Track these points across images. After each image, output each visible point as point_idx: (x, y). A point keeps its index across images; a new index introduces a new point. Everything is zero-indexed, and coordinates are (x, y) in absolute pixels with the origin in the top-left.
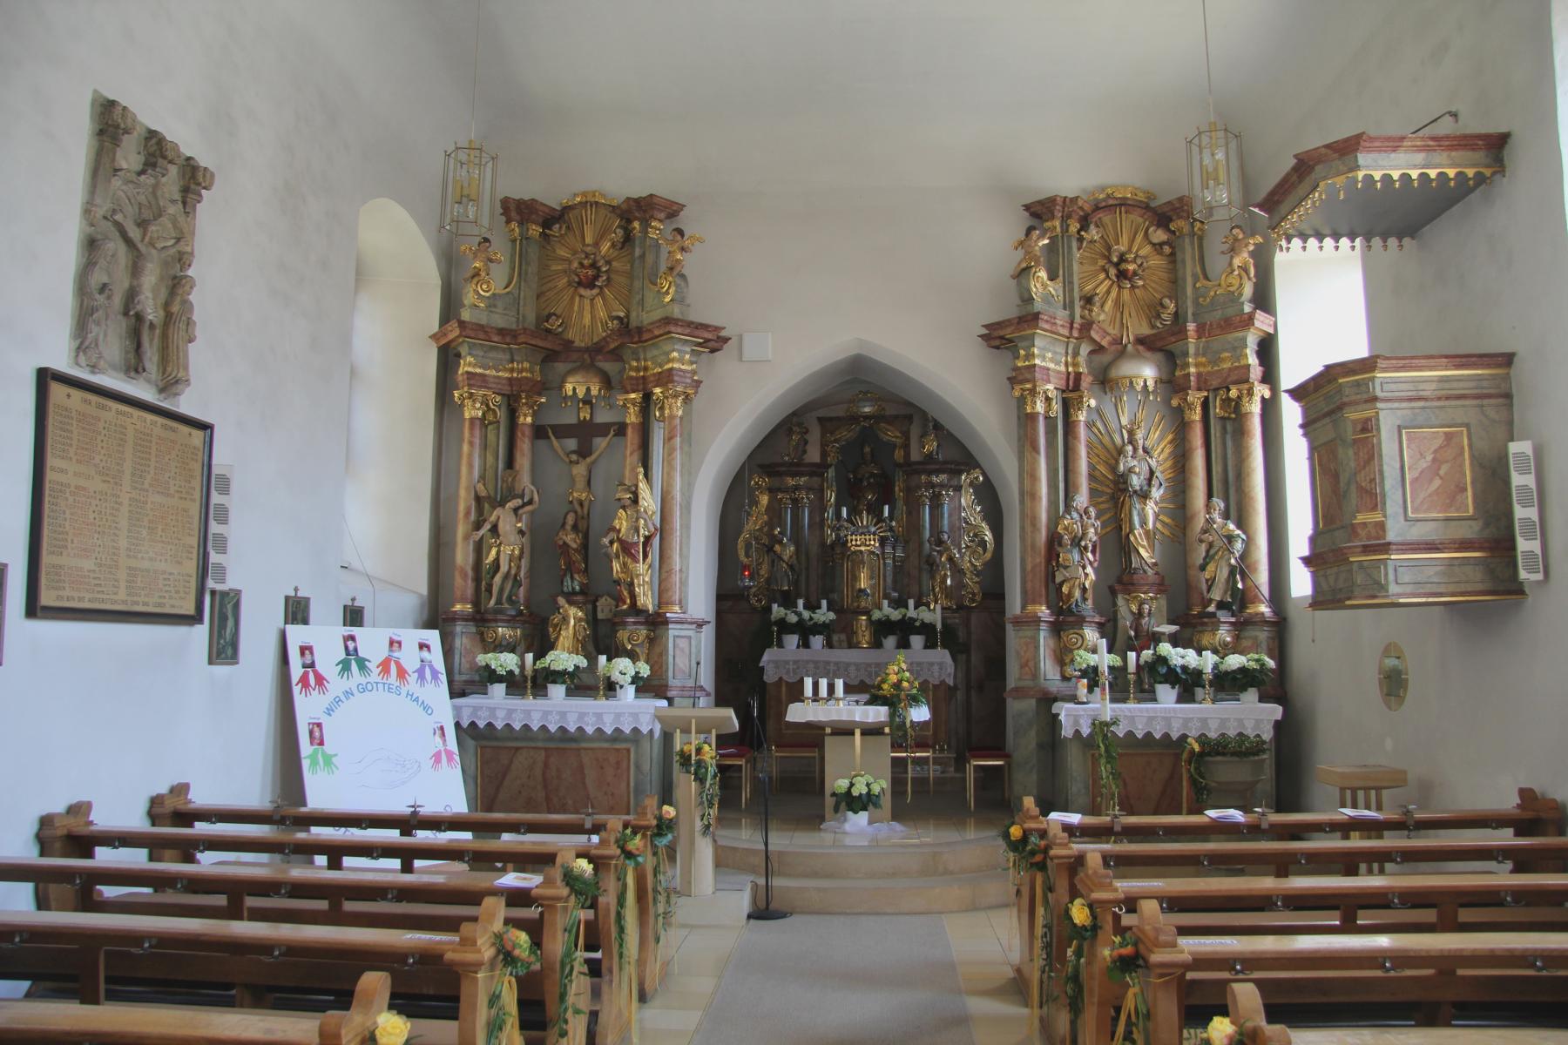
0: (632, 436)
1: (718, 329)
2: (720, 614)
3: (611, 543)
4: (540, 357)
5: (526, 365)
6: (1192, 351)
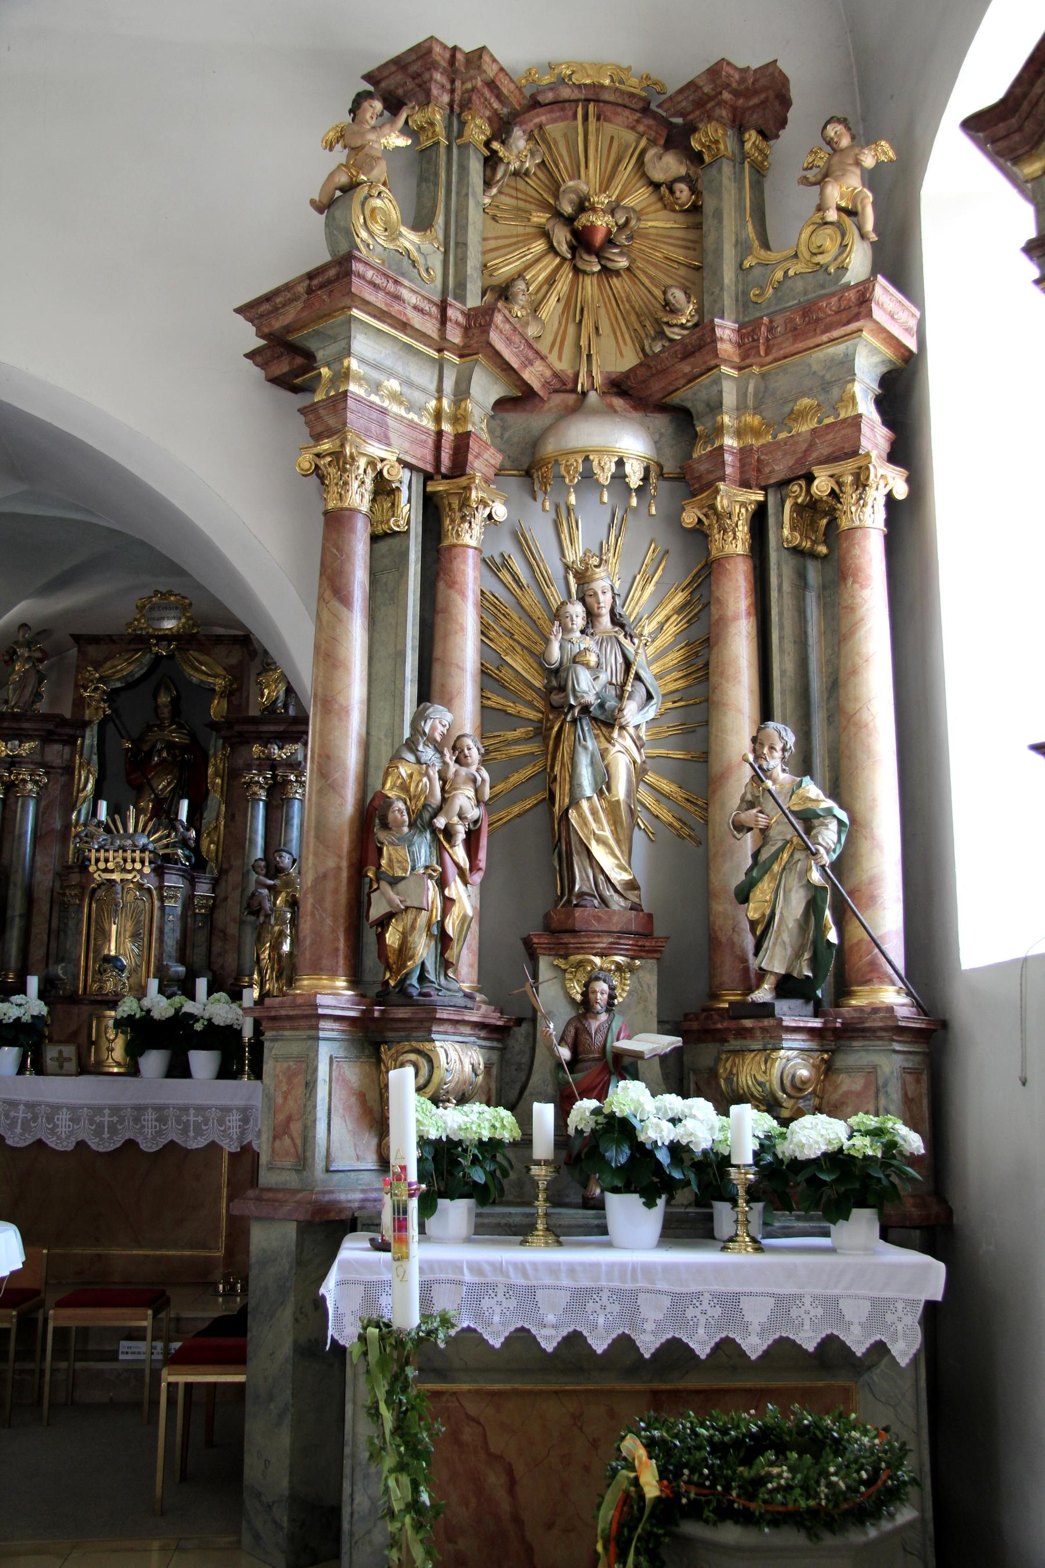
6: (730, 397)
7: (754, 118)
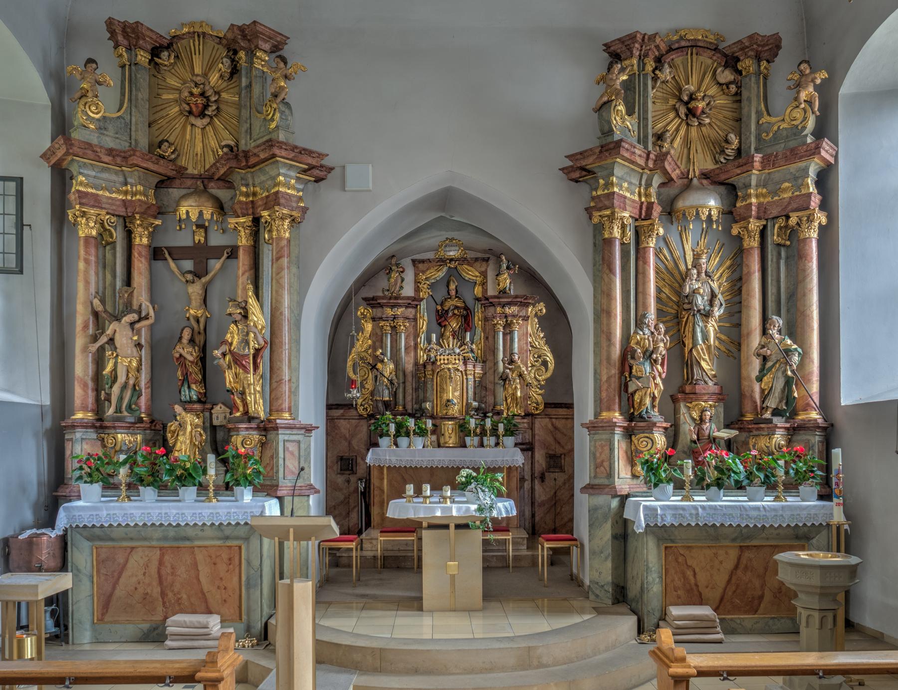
0: (244, 259)
1: (321, 156)
2: (64, 443)
3: (224, 355)
4: (155, 180)
5: (140, 188)
6: (753, 183)
7: (765, 55)
